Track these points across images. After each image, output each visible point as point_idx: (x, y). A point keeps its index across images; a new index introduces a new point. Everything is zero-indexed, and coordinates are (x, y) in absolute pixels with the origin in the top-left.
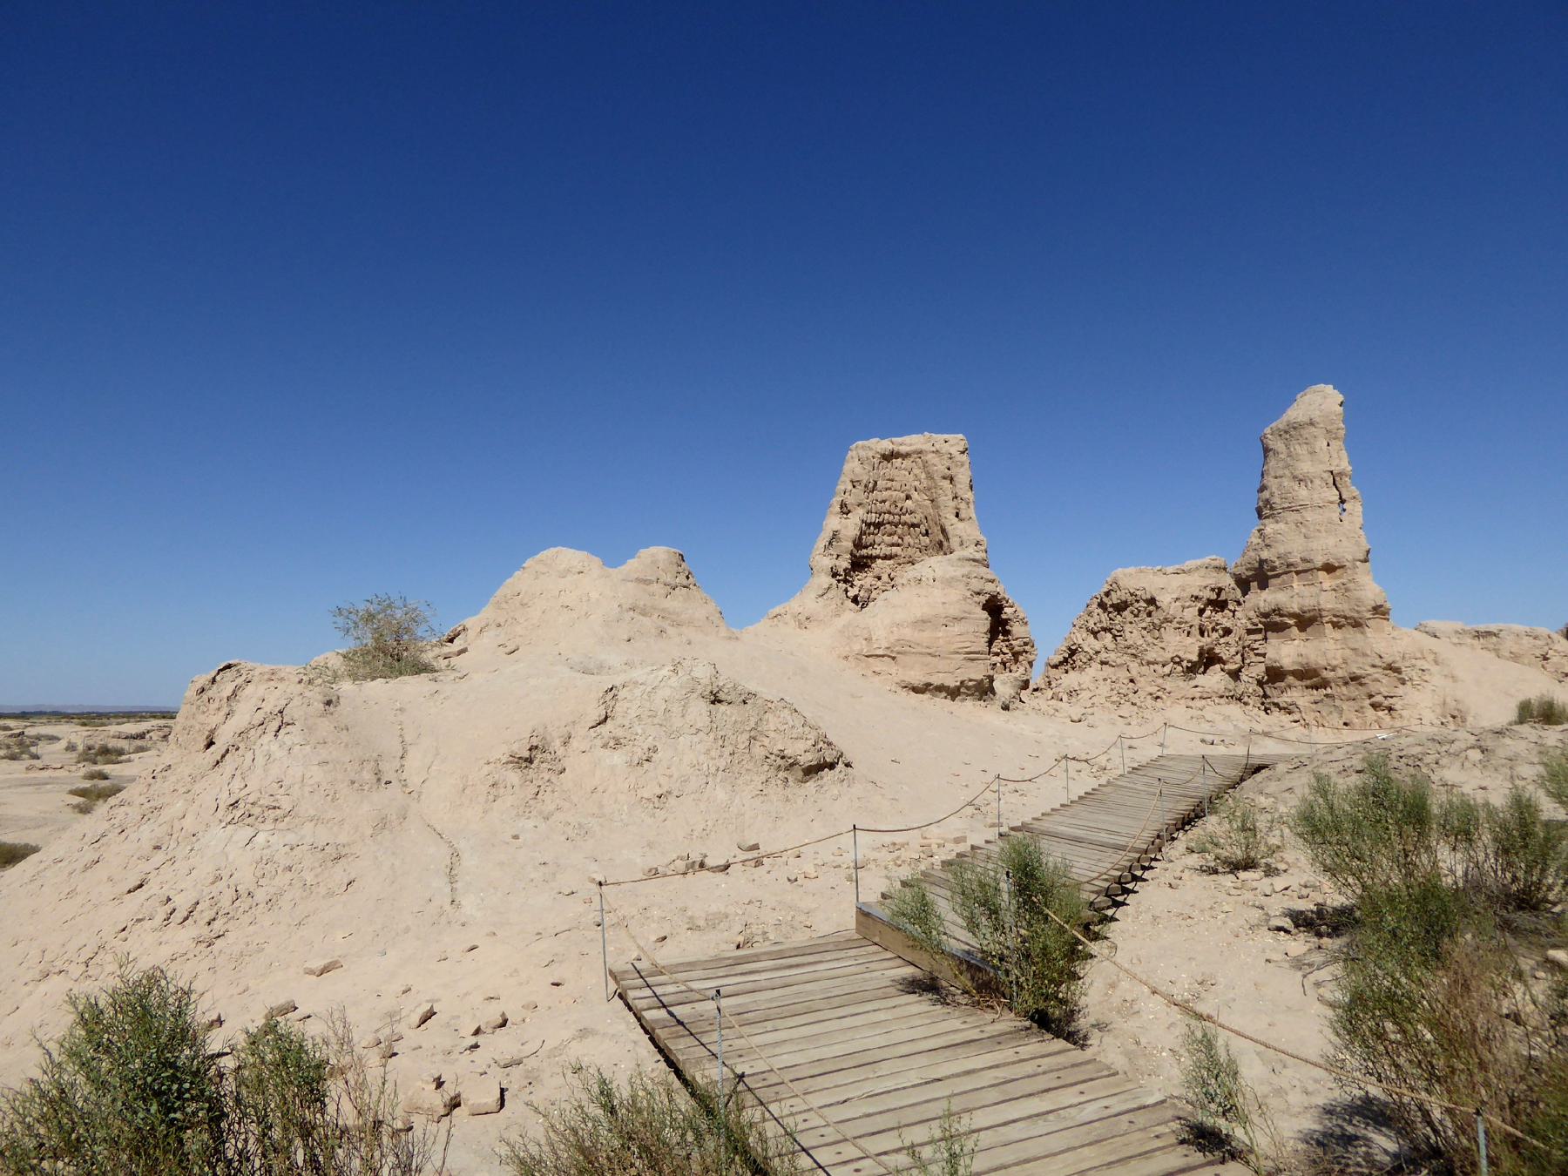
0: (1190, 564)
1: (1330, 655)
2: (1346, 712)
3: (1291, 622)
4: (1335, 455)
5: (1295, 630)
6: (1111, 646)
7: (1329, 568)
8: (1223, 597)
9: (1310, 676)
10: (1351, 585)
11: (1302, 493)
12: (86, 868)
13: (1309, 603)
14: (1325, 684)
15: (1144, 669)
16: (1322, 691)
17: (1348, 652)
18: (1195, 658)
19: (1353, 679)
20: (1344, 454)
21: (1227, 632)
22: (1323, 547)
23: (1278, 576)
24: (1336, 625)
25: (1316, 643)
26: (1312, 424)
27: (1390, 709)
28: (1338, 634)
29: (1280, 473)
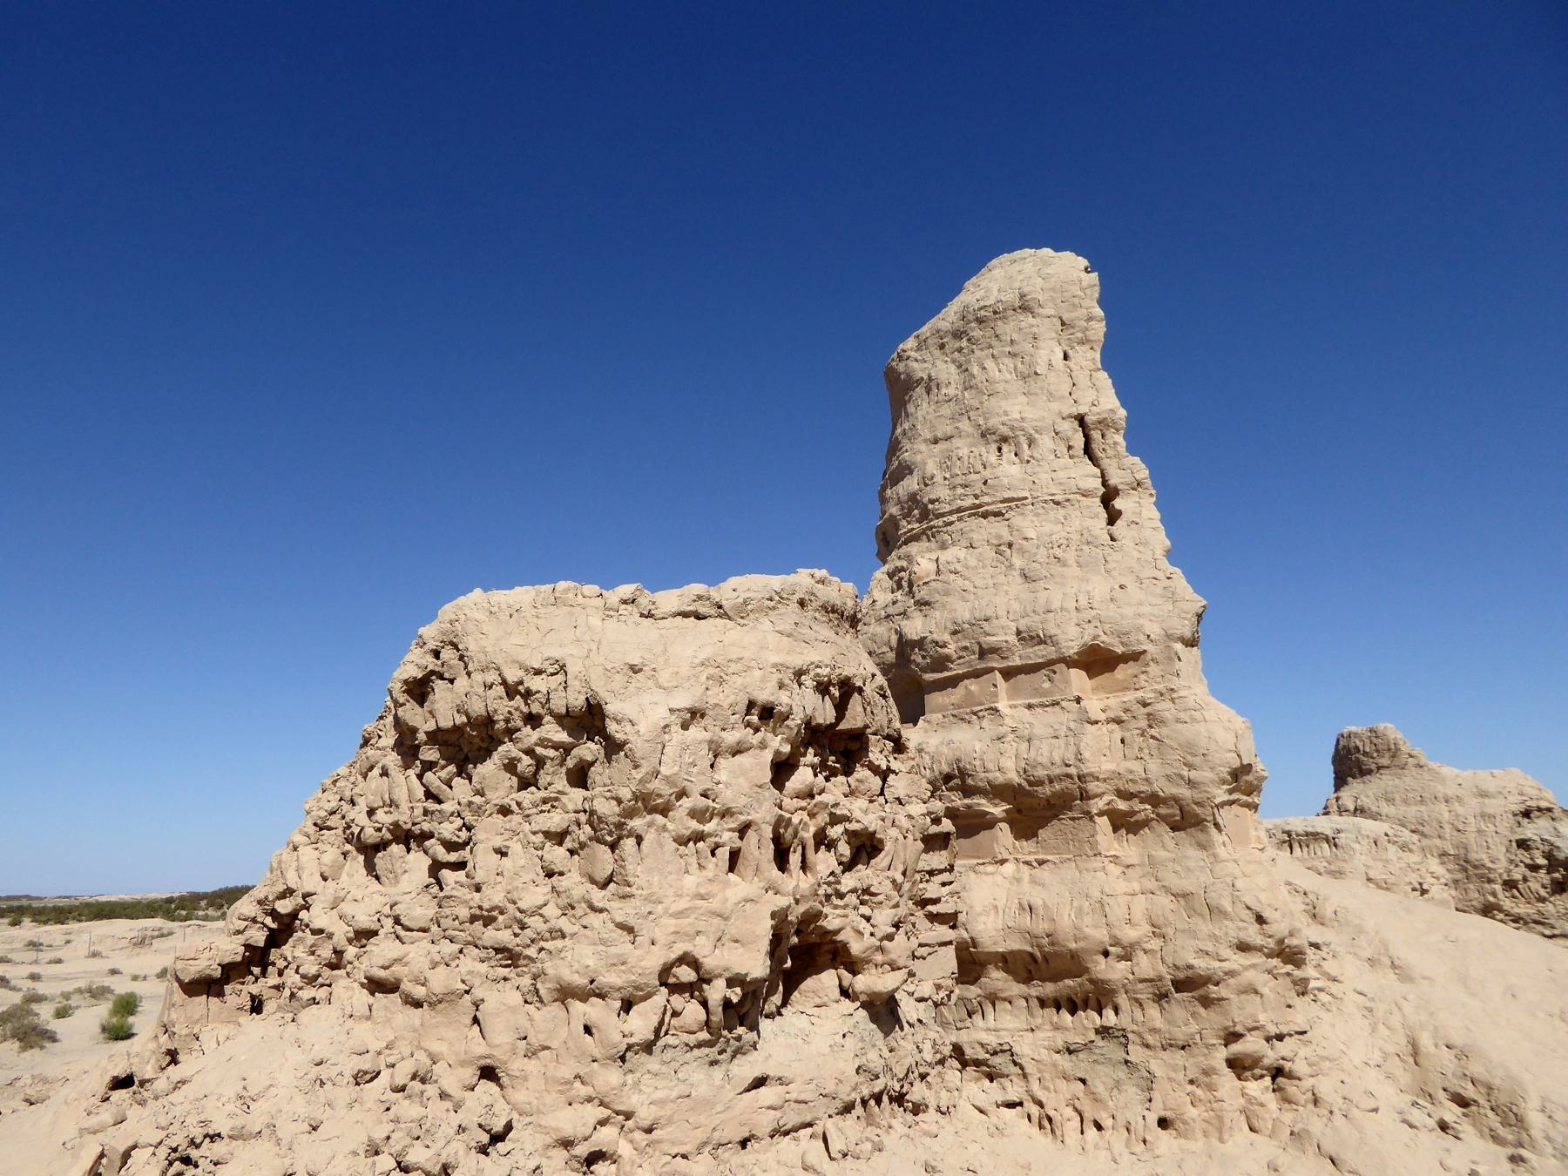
0: (735, 588)
1: (1117, 912)
2: (1161, 1087)
3: (998, 810)
4: (1082, 379)
5: (1004, 832)
6: (419, 910)
7: (1097, 661)
8: (855, 717)
9: (1056, 974)
10: (1164, 708)
11: (1009, 471)
12: (50, 962)
13: (1049, 755)
14: (1098, 997)
15: (547, 1020)
16: (1090, 1019)
17: (1164, 901)
18: (756, 965)
19: (1180, 986)
20: (1104, 378)
21: (866, 847)
22: (1078, 605)
23: (953, 682)
24: (1123, 823)
25: (1070, 871)
26: (1025, 307)
27: (1278, 1072)
28: (1128, 848)
29: (945, 428)
